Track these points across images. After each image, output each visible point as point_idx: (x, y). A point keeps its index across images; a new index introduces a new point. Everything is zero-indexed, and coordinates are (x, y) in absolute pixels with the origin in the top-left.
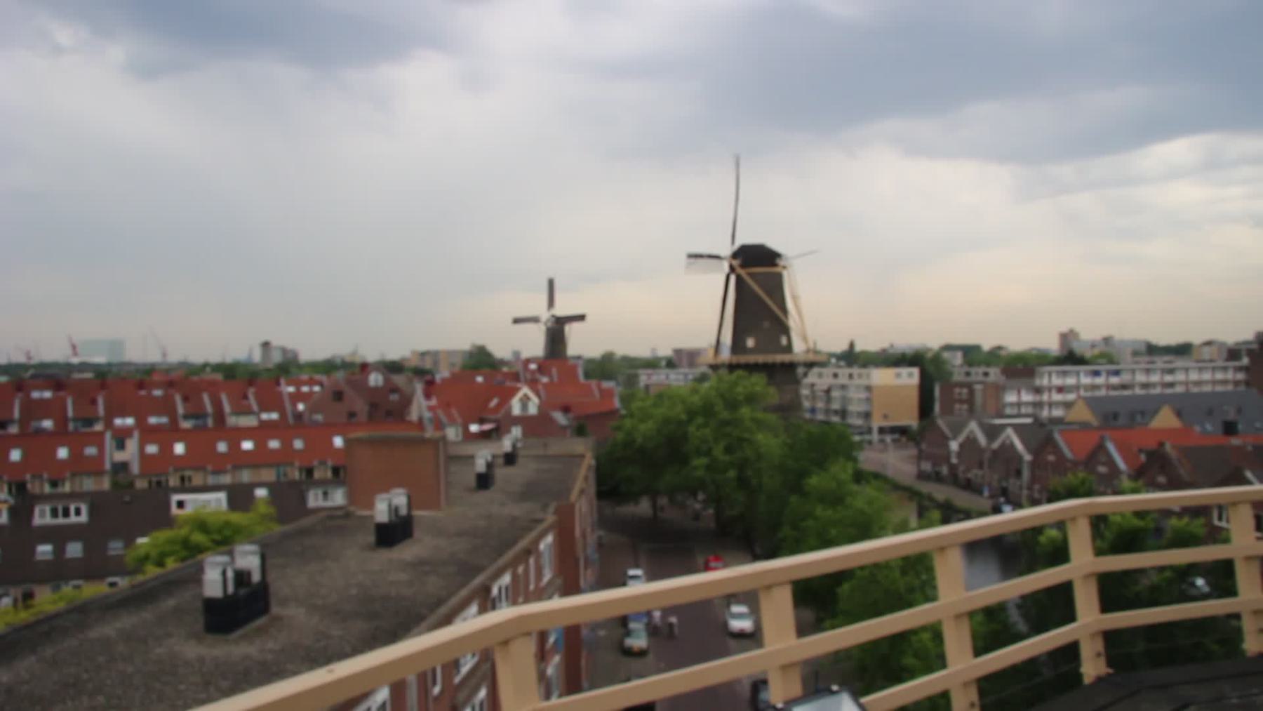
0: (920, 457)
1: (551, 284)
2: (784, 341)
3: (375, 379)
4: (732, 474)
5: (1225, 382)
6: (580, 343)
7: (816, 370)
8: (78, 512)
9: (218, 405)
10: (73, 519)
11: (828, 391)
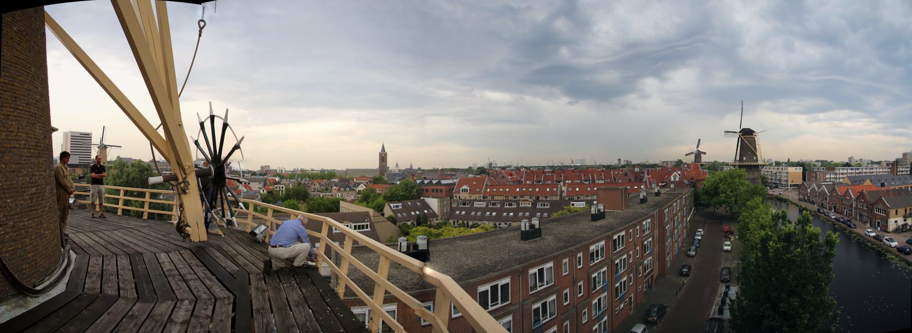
0: (800, 193)
1: (699, 140)
3: (637, 170)
4: (733, 199)
5: (885, 172)
6: (704, 159)
7: (765, 167)
8: (547, 206)
9: (593, 177)
10: (513, 207)
11: (776, 174)
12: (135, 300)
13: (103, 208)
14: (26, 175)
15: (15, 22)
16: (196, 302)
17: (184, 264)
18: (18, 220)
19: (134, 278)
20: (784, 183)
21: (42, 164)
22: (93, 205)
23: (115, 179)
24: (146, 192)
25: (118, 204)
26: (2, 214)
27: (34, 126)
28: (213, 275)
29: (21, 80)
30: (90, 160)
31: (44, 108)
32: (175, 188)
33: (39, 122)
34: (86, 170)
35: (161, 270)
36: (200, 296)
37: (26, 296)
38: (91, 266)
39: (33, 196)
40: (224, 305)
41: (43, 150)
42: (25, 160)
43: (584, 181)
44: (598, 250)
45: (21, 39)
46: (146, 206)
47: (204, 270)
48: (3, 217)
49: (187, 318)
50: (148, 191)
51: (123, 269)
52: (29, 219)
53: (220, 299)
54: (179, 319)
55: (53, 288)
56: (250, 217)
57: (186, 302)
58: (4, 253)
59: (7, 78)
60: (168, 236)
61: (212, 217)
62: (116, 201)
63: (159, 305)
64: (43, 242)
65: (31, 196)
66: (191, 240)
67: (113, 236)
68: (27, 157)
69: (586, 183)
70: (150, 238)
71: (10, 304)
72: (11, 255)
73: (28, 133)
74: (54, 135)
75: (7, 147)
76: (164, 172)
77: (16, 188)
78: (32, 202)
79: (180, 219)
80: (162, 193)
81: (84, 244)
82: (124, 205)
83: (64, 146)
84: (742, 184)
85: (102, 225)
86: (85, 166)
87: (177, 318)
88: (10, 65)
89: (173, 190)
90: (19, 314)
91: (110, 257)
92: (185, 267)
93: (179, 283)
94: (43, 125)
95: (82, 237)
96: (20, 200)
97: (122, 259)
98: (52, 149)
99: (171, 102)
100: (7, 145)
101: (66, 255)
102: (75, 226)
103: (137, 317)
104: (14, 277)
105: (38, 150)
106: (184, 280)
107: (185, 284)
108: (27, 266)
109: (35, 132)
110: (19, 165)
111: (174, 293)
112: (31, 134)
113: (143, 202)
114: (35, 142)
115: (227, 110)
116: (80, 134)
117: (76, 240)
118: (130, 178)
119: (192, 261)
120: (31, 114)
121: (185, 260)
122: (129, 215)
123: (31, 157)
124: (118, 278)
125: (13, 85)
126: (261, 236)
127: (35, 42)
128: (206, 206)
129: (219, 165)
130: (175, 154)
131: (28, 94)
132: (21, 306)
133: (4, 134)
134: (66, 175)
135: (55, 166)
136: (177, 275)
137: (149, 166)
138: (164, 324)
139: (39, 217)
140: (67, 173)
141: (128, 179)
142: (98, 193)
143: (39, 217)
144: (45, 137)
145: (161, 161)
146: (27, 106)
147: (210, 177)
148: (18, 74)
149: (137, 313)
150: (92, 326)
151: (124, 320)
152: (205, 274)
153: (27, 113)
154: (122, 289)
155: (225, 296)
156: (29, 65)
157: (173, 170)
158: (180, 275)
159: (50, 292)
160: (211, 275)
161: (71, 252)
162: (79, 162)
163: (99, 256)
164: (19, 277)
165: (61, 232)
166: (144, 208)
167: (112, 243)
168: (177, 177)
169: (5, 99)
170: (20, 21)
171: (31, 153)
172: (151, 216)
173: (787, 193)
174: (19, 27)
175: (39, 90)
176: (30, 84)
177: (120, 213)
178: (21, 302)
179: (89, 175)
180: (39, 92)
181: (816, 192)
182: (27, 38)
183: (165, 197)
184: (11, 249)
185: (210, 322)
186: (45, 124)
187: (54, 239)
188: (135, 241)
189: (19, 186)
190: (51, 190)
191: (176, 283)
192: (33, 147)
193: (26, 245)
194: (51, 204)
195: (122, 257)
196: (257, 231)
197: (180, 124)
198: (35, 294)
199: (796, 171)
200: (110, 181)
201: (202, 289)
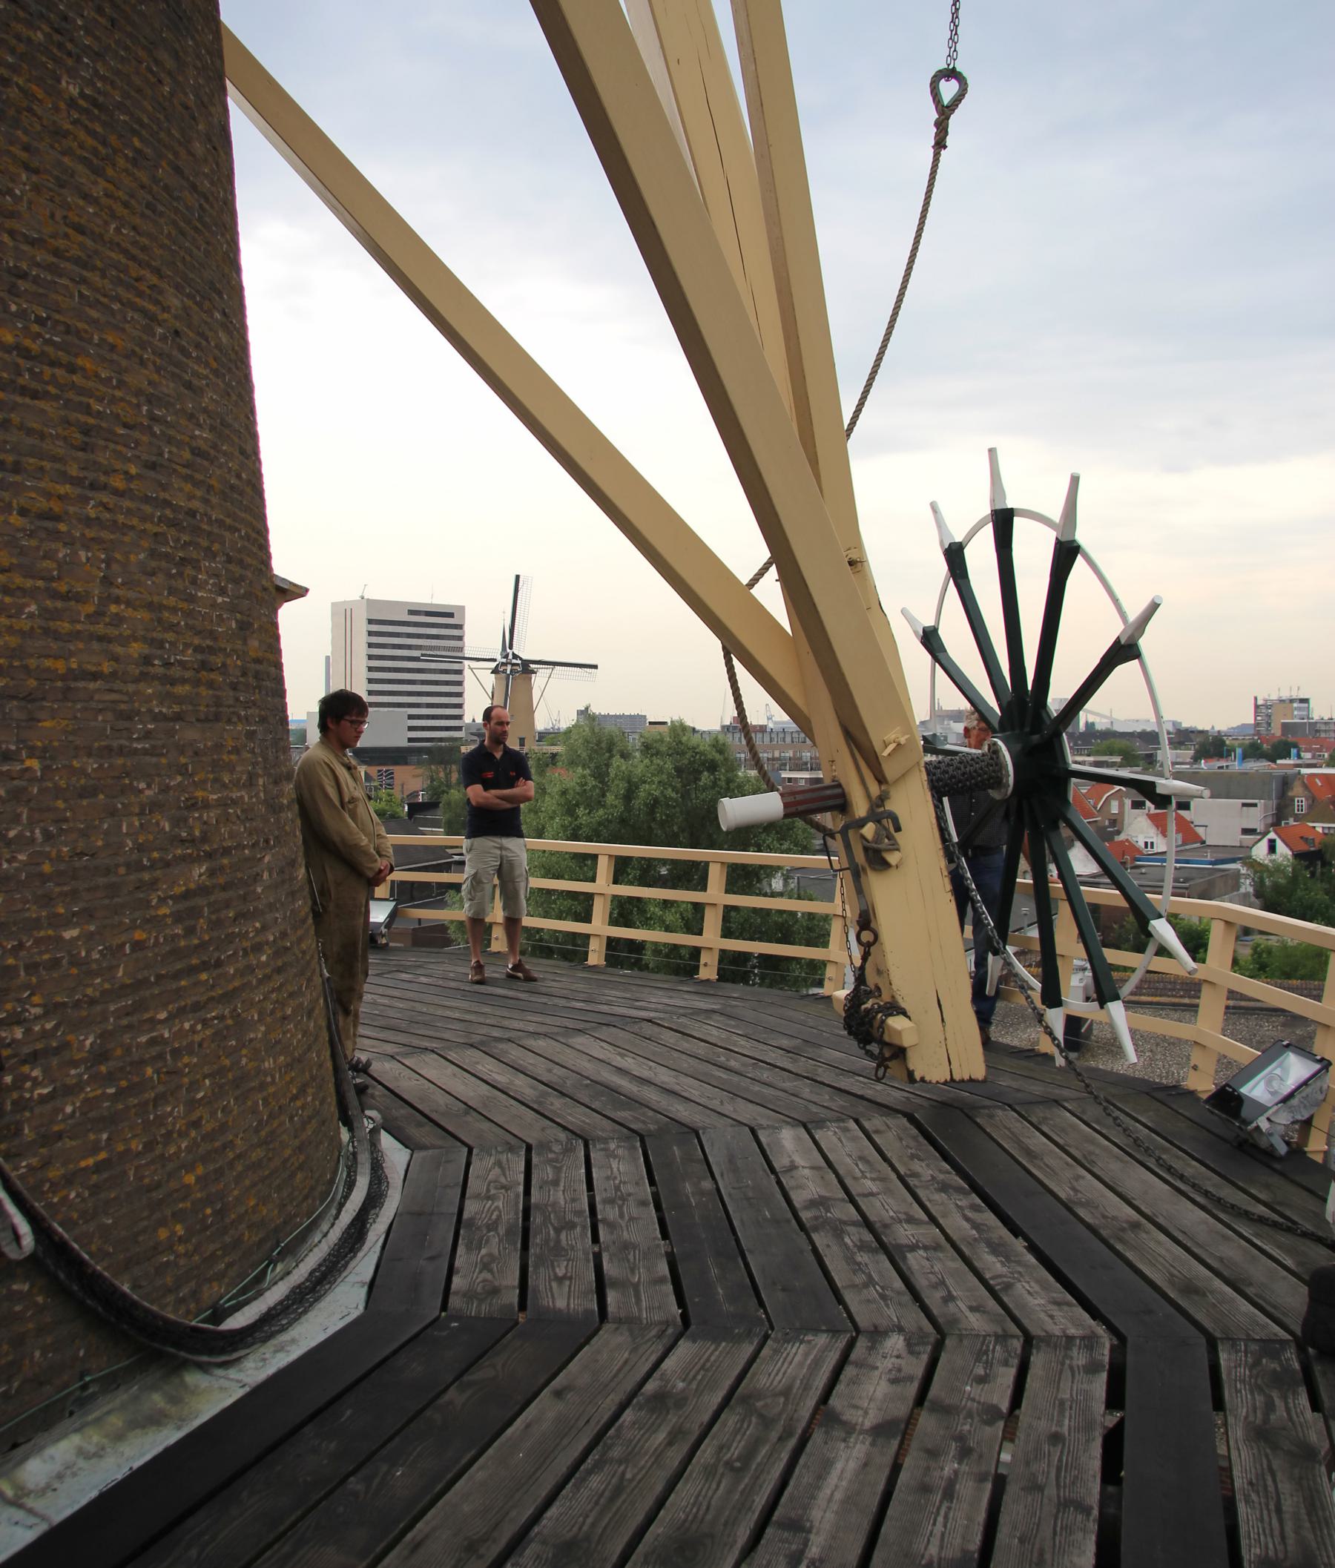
12: (670, 1331)
13: (522, 940)
14: (155, 806)
15: (70, 54)
16: (938, 1348)
17: (883, 1179)
18: (125, 1022)
19: (665, 1235)
21: (236, 750)
22: (479, 927)
23: (570, 810)
24: (707, 864)
25: (587, 918)
26: (36, 999)
27: (189, 571)
28: (1016, 1232)
29: (113, 348)
30: (459, 728)
31: (232, 487)
32: (836, 844)
33: (212, 555)
34: (442, 775)
35: (785, 1205)
36: (954, 1321)
37: (183, 1365)
38: (477, 1196)
39: (200, 901)
40: (1067, 1373)
41: (234, 687)
42: (147, 735)
45: (104, 143)
46: (712, 922)
47: (974, 1208)
48: (46, 1016)
49: (902, 1410)
50: (717, 859)
51: (618, 1199)
52: (181, 1012)
53: (1048, 1339)
54: (866, 1413)
55: (305, 1312)
56: (1211, 1007)
57: (895, 1342)
58: (55, 1187)
59: (36, 328)
60: (810, 1052)
61: (1009, 976)
62: (581, 907)
63: (776, 1351)
64: (254, 1111)
65: (182, 906)
66: (910, 1075)
67: (568, 1057)
68: (157, 718)
70: (733, 1063)
71: (98, 1421)
72: (95, 1190)
73: (161, 607)
74: (288, 615)
75: (48, 670)
76: (785, 775)
77: (108, 871)
78: (190, 931)
79: (860, 978)
80: (779, 868)
81: (442, 1099)
82: (614, 922)
83: (338, 669)
85: (516, 1014)
86: (439, 754)
87: (856, 1407)
88: (50, 268)
89: (826, 850)
90: (148, 1457)
91: (557, 1148)
92: (888, 1191)
93: (862, 1258)
94: (231, 567)
95: (433, 1069)
96: (133, 927)
97: (611, 1155)
98: (280, 680)
99: (814, 461)
100: (48, 663)
101: (364, 1159)
102: (404, 1025)
103: (681, 1401)
104: (115, 1290)
105: (211, 685)
106: (883, 1247)
107: (887, 1264)
108: (179, 1229)
109: (192, 599)
110: (120, 761)
111: (840, 1300)
112: (174, 610)
113: (699, 908)
114: (198, 649)
115: (1075, 481)
116: (412, 612)
117: (407, 1085)
118: (637, 803)
119: (917, 1166)
120: (168, 512)
121: (885, 1159)
122: (639, 965)
123: (178, 717)
124: (595, 1239)
125: (72, 369)
126: (1284, 1118)
127: (178, 170)
128: (978, 924)
129: (1036, 738)
130: (831, 691)
131: (154, 419)
132: (156, 1420)
133: (33, 608)
134: (353, 800)
135: (298, 758)
136: (854, 1224)
137: (719, 747)
138: (799, 1431)
139: (228, 997)
140: (353, 789)
141: (628, 808)
142: (499, 871)
143: (228, 997)
144: (244, 626)
145: (771, 725)
146: (151, 474)
147: (995, 794)
148: (94, 314)
149: (681, 1385)
150: (490, 1451)
151: (628, 1416)
152: (975, 1226)
153: (148, 509)
154: (617, 1284)
155: (1072, 1331)
156: (154, 280)
157: (825, 764)
158: (868, 1224)
159: (294, 1332)
160: (1004, 1232)
161: (386, 1140)
162: (410, 740)
163: (511, 1149)
164: (133, 1288)
165: (334, 1056)
166: (700, 933)
167: (568, 1088)
168: (843, 795)
169: (30, 432)
170: (98, 56)
171: (179, 700)
172: (734, 967)
174: (91, 83)
175: (205, 402)
176: (158, 370)
177: (596, 955)
178: (157, 1399)
179: (455, 795)
180: (205, 411)
182: (137, 143)
183: (793, 884)
184: (91, 1161)
185: (1004, 1438)
186: (241, 563)
187: (303, 1090)
188: (665, 1077)
189: (121, 860)
190: (282, 871)
191: (850, 1260)
192: (188, 674)
193: (170, 1133)
194: (284, 935)
195: (612, 1146)
196: (1256, 1090)
197: (854, 556)
198: (222, 1351)
200: (552, 818)
201: (965, 1292)
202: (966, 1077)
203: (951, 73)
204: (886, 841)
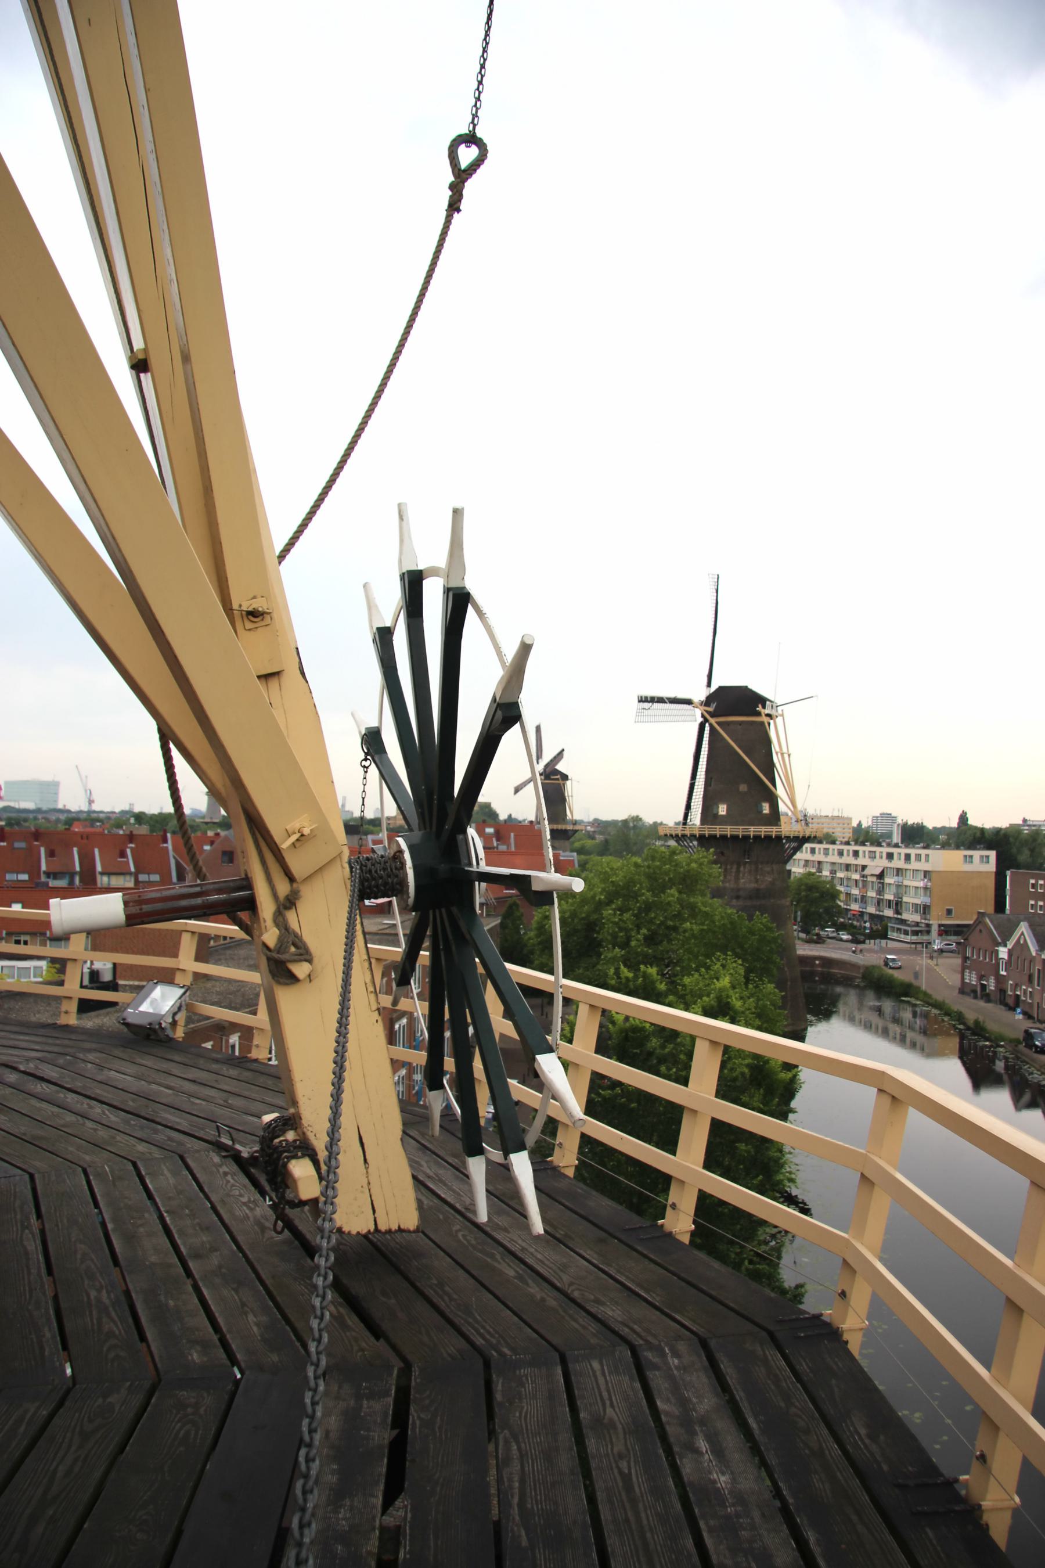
2: (766, 808)
7: (807, 846)
11: (881, 876)
20: (916, 918)
43: (48, 874)
44: (811, 1215)
69: (53, 883)
84: (694, 912)
173: (923, 962)
181: (1032, 960)
199: (968, 868)
202: (394, 1227)
203: (470, 138)
204: (293, 949)
